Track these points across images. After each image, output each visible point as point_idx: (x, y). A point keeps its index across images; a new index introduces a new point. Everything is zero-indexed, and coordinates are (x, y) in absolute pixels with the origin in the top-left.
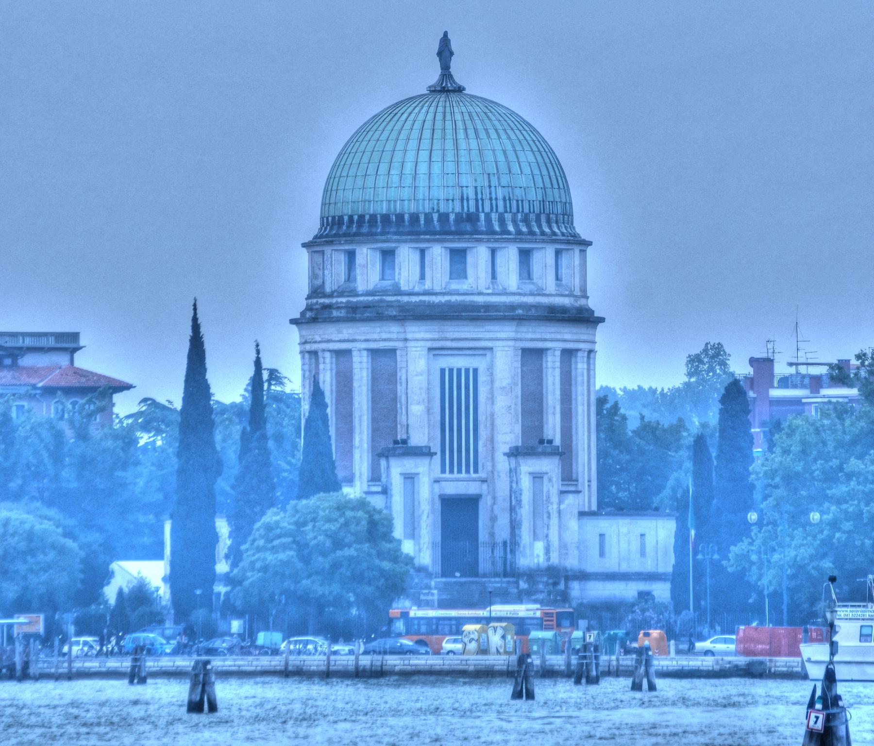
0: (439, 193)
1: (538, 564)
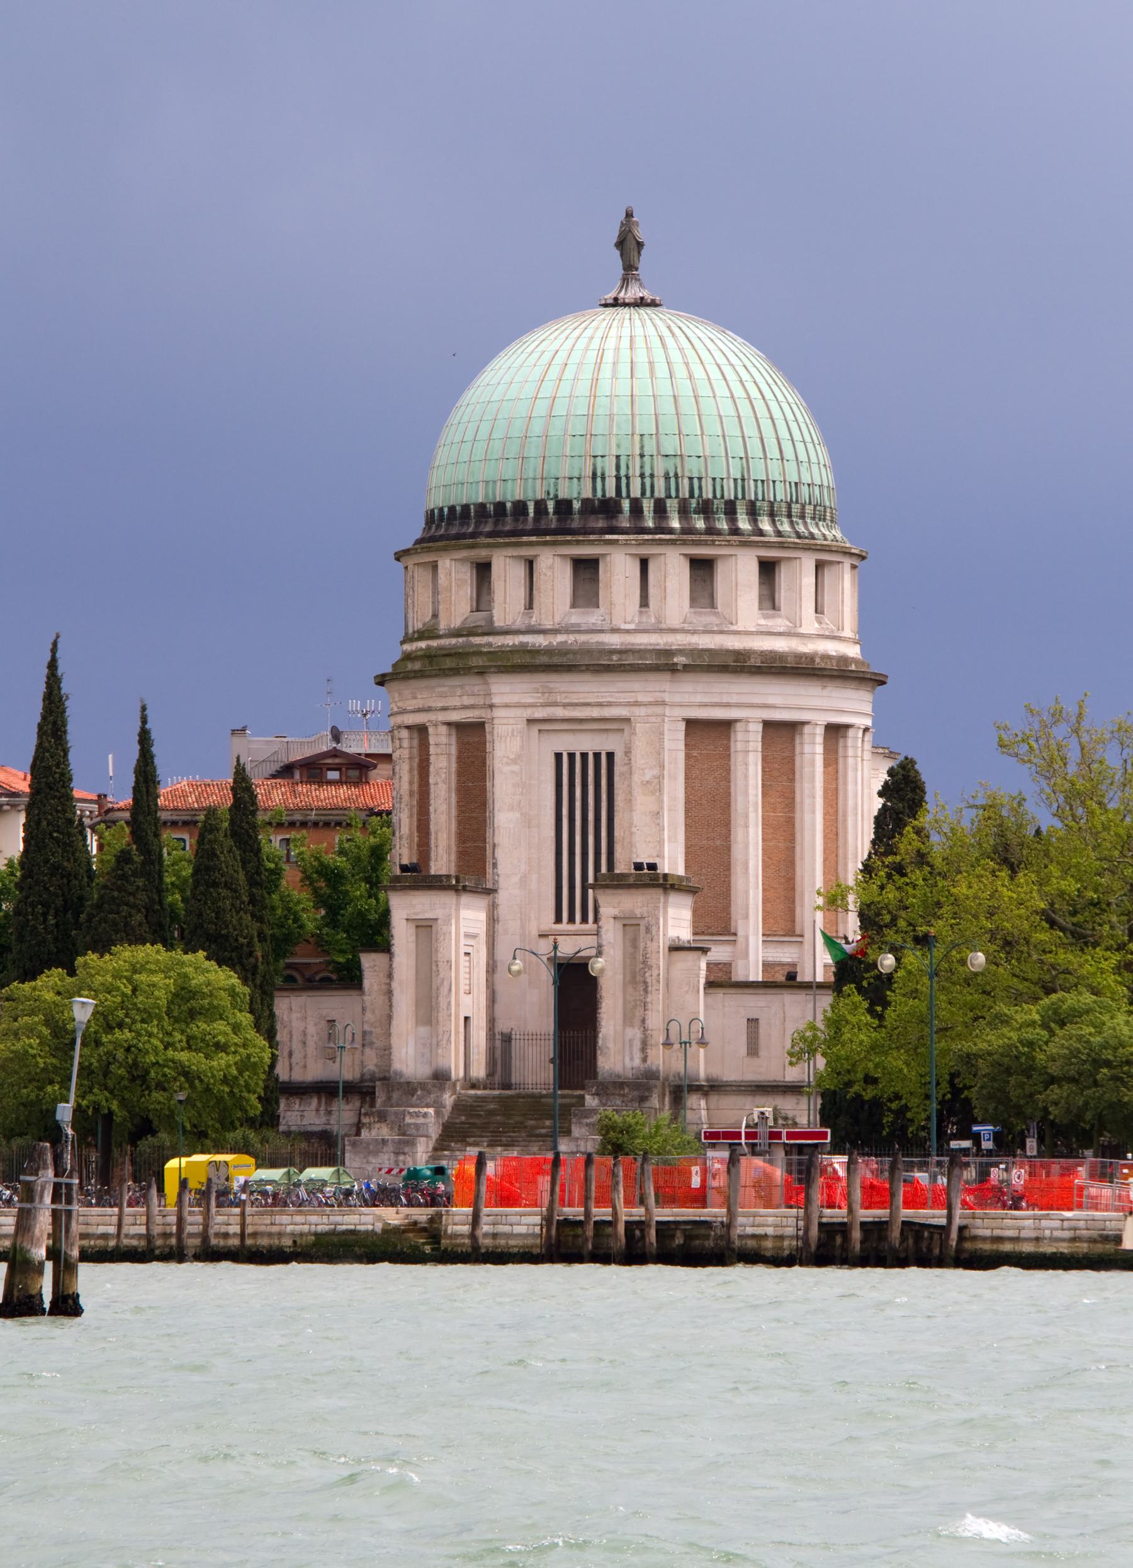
0: (718, 470)
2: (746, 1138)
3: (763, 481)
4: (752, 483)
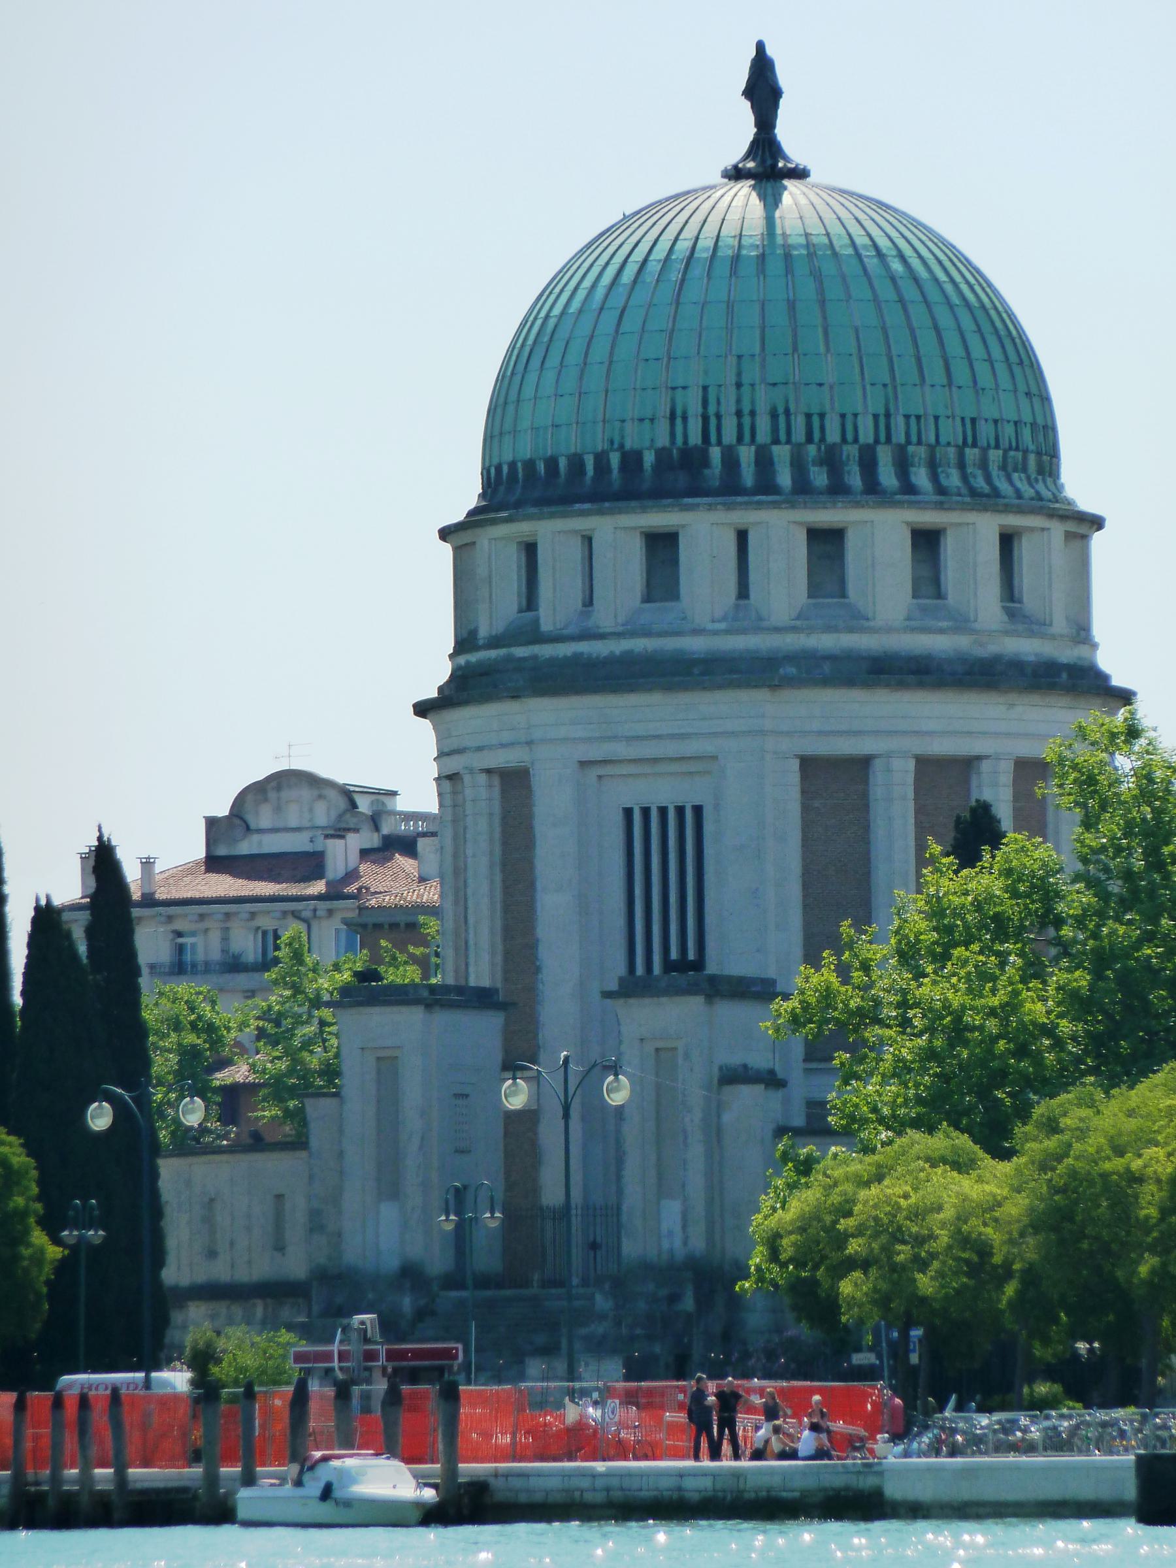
1: (671, 1250)
2: (340, 1361)
3: (918, 417)
4: (901, 420)
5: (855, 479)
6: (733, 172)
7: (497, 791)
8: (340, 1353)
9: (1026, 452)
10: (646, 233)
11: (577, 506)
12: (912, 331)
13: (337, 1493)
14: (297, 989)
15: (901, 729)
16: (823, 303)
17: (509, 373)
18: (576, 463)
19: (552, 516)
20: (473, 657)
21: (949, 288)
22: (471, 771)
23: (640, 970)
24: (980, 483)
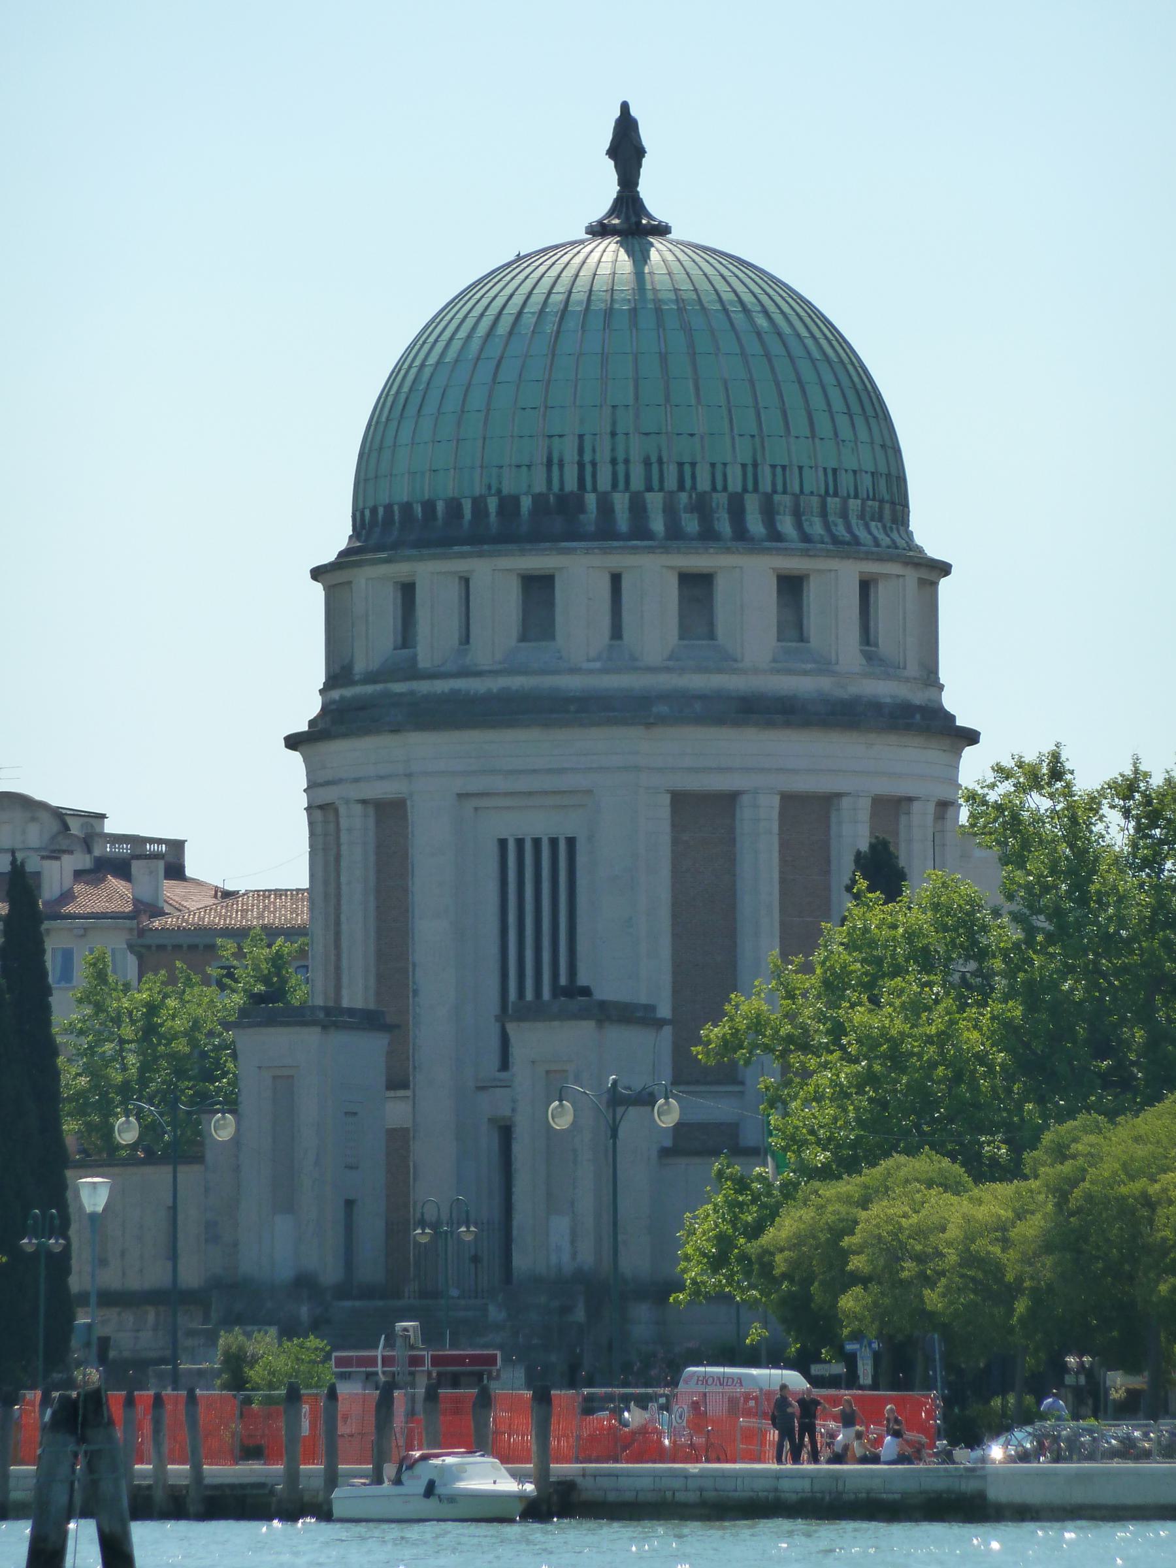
2: (383, 1365)
3: (784, 468)
4: (768, 471)
5: (724, 526)
6: (599, 229)
7: (371, 822)
8: (383, 1357)
9: (882, 501)
10: (520, 285)
11: (456, 549)
12: (777, 384)
13: (440, 1490)
14: (99, 1008)
15: (767, 766)
16: (693, 355)
17: (384, 419)
18: (454, 507)
19: (434, 557)
20: (348, 692)
21: (809, 342)
22: (347, 802)
23: (529, 995)
24: (841, 531)
